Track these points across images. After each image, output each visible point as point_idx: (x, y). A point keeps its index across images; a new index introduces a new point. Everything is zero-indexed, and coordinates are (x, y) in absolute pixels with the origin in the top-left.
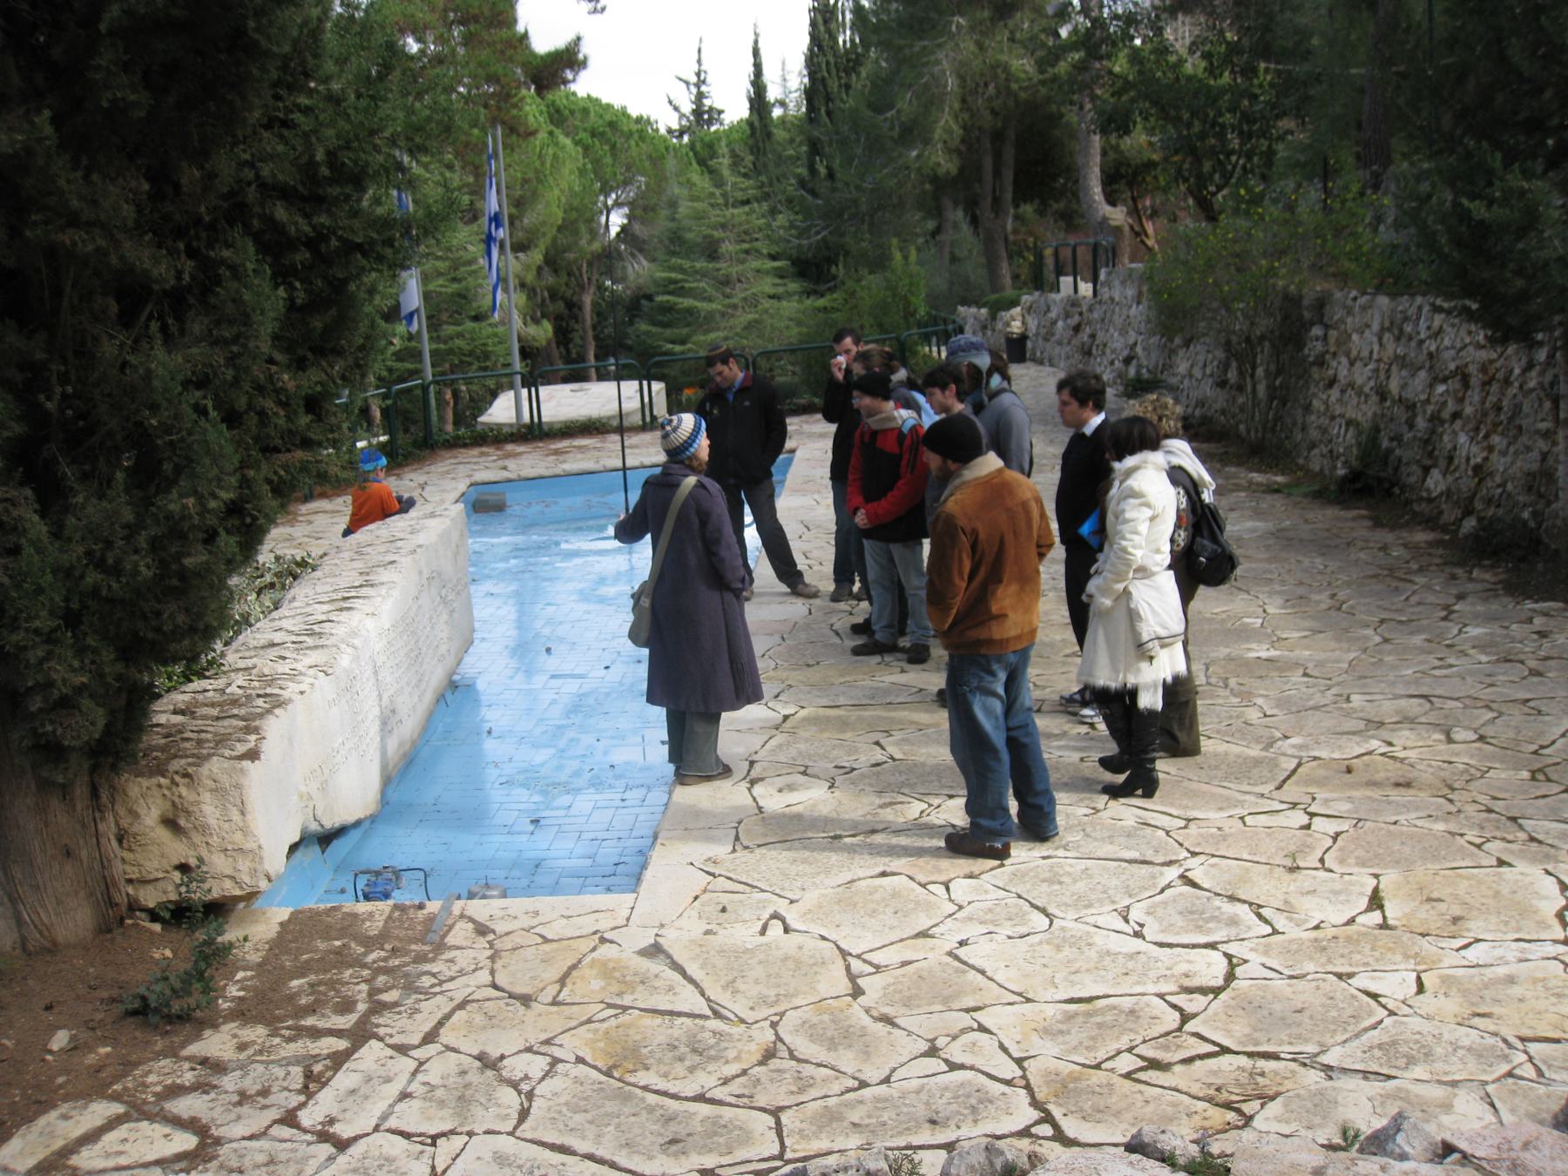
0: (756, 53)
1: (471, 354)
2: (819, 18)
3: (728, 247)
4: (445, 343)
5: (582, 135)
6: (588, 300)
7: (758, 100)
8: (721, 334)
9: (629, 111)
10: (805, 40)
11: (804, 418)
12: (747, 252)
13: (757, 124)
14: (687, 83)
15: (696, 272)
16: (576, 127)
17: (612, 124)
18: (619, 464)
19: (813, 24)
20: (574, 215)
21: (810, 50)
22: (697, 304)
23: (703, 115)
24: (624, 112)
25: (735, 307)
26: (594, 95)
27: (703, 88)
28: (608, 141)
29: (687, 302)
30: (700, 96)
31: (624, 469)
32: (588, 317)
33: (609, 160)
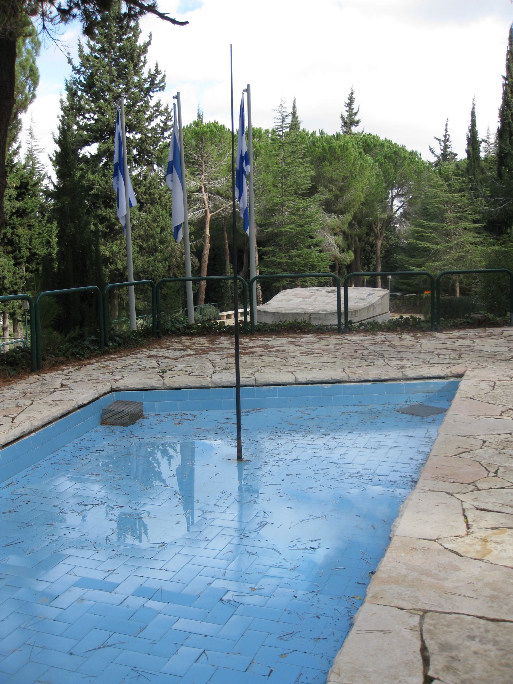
0: (473, 114)
1: (305, 265)
2: (509, 89)
3: (450, 215)
4: (291, 259)
5: (379, 157)
6: (379, 243)
7: (473, 141)
8: (442, 263)
9: (406, 148)
10: (499, 102)
11: (478, 331)
12: (460, 218)
13: (471, 152)
14: (439, 140)
15: (431, 228)
16: (377, 154)
17: (395, 153)
18: (230, 378)
19: (505, 93)
20: (372, 198)
21: (503, 107)
22: (429, 245)
23: (446, 155)
24: (403, 148)
25: (451, 248)
26: (388, 139)
27: (448, 143)
28: (393, 161)
29: (423, 244)
30: (446, 147)
31: (238, 386)
32: (379, 252)
33: (393, 171)
